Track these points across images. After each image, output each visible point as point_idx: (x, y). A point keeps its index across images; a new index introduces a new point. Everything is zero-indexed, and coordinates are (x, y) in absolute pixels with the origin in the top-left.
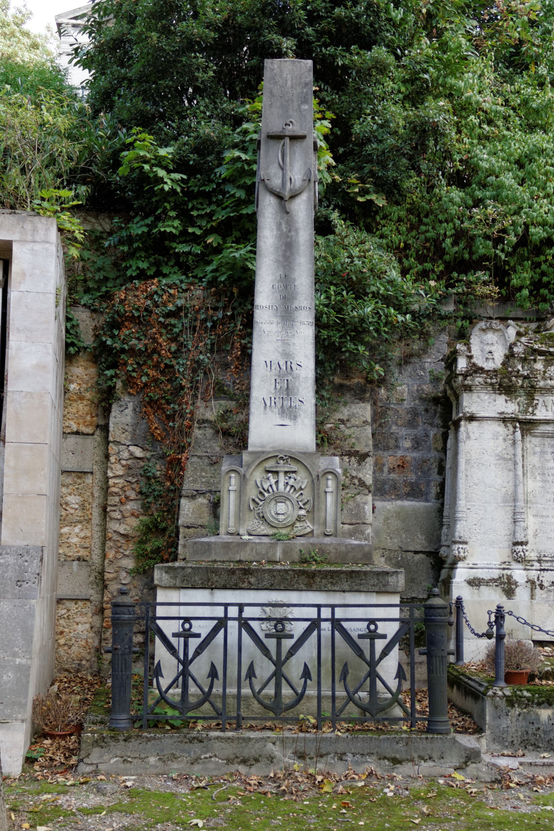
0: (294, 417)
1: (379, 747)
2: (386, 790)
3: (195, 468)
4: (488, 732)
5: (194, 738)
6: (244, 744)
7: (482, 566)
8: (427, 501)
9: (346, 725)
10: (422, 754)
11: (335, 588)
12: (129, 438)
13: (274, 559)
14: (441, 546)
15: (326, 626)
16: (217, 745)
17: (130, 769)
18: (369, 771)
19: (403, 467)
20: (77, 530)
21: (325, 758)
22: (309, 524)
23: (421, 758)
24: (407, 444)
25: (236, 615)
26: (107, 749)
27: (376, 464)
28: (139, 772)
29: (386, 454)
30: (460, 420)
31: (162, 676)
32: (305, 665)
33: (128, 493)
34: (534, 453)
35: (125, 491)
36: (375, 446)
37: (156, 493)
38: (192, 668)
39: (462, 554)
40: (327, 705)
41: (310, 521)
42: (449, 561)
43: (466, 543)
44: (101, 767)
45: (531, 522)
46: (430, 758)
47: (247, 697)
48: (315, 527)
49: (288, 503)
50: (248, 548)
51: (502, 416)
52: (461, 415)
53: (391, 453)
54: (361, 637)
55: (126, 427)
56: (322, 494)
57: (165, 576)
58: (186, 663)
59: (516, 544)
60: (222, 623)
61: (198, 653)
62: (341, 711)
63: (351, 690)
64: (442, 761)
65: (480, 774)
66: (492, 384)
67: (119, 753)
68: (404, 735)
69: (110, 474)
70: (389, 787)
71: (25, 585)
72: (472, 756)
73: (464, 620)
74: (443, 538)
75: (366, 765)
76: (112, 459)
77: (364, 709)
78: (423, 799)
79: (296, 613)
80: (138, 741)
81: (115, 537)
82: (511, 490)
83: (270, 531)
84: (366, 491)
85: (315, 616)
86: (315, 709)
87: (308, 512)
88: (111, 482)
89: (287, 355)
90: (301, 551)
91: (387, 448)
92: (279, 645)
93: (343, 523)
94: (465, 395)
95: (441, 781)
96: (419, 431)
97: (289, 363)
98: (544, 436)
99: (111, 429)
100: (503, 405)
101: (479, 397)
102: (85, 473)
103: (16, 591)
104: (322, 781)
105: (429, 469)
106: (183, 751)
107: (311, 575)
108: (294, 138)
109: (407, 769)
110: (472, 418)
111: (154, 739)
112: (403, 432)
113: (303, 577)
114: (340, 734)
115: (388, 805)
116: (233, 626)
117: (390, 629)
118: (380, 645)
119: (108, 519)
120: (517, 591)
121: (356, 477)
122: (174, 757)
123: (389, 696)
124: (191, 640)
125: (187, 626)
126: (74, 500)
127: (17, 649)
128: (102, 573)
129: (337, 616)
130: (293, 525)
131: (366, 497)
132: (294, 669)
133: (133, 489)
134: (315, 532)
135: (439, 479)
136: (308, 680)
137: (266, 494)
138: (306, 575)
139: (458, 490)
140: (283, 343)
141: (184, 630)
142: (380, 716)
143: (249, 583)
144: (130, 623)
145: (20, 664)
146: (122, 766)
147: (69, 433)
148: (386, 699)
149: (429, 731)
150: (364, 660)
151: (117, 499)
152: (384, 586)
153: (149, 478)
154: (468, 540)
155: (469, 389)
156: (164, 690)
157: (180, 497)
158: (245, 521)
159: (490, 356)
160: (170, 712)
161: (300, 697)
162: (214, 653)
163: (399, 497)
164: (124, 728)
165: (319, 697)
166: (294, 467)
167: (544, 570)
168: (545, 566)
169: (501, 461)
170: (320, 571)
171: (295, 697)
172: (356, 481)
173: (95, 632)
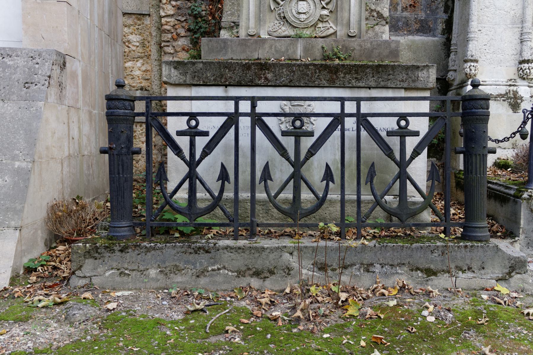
1: (411, 256)
2: (425, 313)
3: (233, 3)
4: (522, 237)
5: (200, 248)
6: (257, 255)
7: (491, 83)
9: (372, 231)
10: (460, 264)
11: (360, 84)
13: (294, 57)
15: (350, 123)
16: (227, 255)
17: (128, 283)
18: (401, 285)
19: (414, 7)
20: (139, 64)
21: (349, 269)
22: (332, 25)
23: (459, 268)
25: (249, 111)
26: (101, 261)
28: (138, 286)
33: (179, 31)
35: (176, 29)
37: (202, 30)
38: (199, 170)
40: (351, 210)
41: (333, 22)
42: (456, 83)
43: (476, 61)
44: (95, 280)
46: (469, 269)
47: (263, 203)
48: (339, 28)
50: (267, 46)
57: (174, 73)
58: (192, 164)
59: (521, 62)
61: (206, 153)
62: (367, 216)
63: (378, 193)
64: (483, 272)
65: (526, 286)
67: (115, 265)
68: (439, 244)
70: (427, 308)
71: (33, 87)
74: (450, 64)
75: (396, 278)
77: (390, 213)
78: (474, 327)
79: (317, 107)
80: (137, 252)
82: (519, 12)
83: (290, 32)
84: (384, 22)
86: (338, 214)
87: (331, 12)
90: (323, 48)
92: (297, 144)
95: (485, 297)
102: (144, 15)
103: (23, 93)
104: (347, 300)
105: (437, 8)
106: (187, 262)
107: (334, 71)
109: (443, 281)
111: (154, 249)
113: (325, 72)
114: (366, 243)
115: (432, 339)
116: (245, 123)
119: (163, 54)
121: (375, 10)
122: (177, 270)
123: (422, 200)
125: (193, 123)
127: (17, 152)
130: (315, 26)
131: (383, 28)
132: (314, 171)
133: (183, 27)
134: (338, 33)
135: (445, 17)
136: (331, 183)
138: (330, 70)
139: (471, 12)
141: (190, 127)
142: (411, 221)
143: (266, 78)
145: (19, 167)
146: (118, 279)
148: (414, 203)
149: (464, 237)
150: (394, 160)
151: (170, 36)
152: (414, 81)
153: (196, 17)
154: (479, 59)
157: (220, 29)
158: (265, 22)
160: (181, 219)
161: (321, 201)
164: (123, 237)
165: (343, 201)
170: (343, 65)
171: (316, 202)
172: (375, 14)
173: (158, 150)
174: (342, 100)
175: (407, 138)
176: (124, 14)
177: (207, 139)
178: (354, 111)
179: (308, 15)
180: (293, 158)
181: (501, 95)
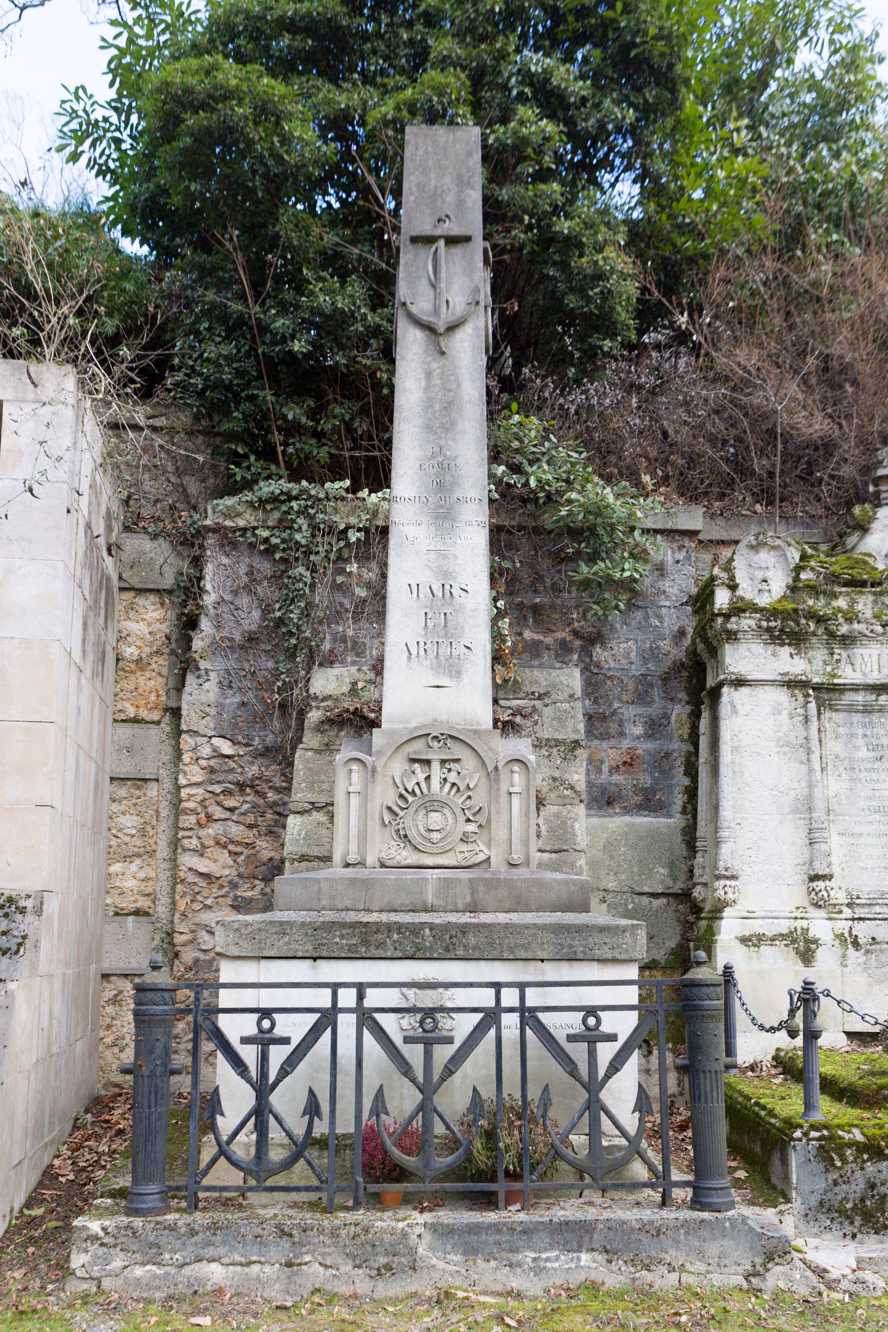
0: (456, 672)
7: (763, 914)
8: (670, 816)
12: (212, 725)
14: (695, 884)
15: (510, 1021)
20: (134, 867)
22: (482, 847)
24: (638, 730)
25: (353, 1004)
27: (590, 761)
29: (605, 745)
30: (720, 685)
31: (222, 1114)
32: (475, 1089)
33: (210, 810)
34: (837, 737)
36: (589, 732)
38: (275, 1099)
39: (730, 896)
43: (733, 877)
45: (835, 844)
49: (447, 811)
51: (786, 679)
52: (722, 677)
53: (612, 742)
54: (571, 1038)
55: (207, 709)
56: (504, 798)
58: (263, 1089)
60: (327, 1018)
61: (284, 1072)
66: (769, 630)
69: (182, 781)
72: (776, 1252)
73: (737, 1002)
76: (186, 758)
81: (191, 878)
85: (492, 1004)
88: (184, 793)
89: (445, 574)
91: (605, 736)
92: (428, 1056)
93: (540, 851)
94: (727, 646)
96: (655, 710)
97: (447, 587)
98: (851, 709)
99: (184, 712)
100: (788, 662)
101: (749, 650)
102: (146, 780)
108: (452, 241)
110: (739, 682)
112: (630, 712)
116: (347, 1023)
117: (623, 1024)
118: (606, 1052)
120: (819, 953)
123: (624, 1142)
124: (273, 1048)
125: (266, 1024)
126: (130, 822)
128: (170, 934)
129: (529, 1003)
134: (493, 860)
137: (410, 799)
139: (721, 795)
140: (436, 548)
141: (261, 1031)
144: (165, 1021)
147: (123, 721)
148: (610, 1149)
150: (579, 1080)
151: (193, 819)
155: (732, 636)
156: (225, 1138)
159: (764, 586)
162: (313, 1070)
163: (626, 811)
166: (458, 751)
167: (860, 919)
168: (860, 912)
169: (787, 749)
174: (497, 986)
175: (599, 1045)
176: (112, 779)
177: (288, 1050)
178: (516, 1003)
179: (444, 834)
180: (420, 1078)
181: (781, 935)
